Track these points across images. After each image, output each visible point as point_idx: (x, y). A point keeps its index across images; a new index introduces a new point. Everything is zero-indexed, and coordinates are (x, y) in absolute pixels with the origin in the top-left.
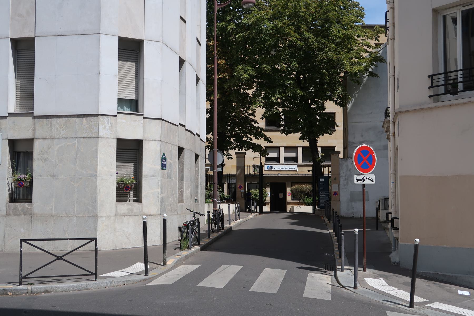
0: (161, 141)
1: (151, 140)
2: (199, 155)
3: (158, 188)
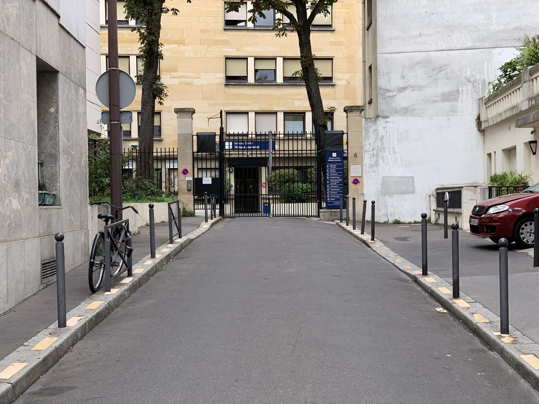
2: (58, 72)
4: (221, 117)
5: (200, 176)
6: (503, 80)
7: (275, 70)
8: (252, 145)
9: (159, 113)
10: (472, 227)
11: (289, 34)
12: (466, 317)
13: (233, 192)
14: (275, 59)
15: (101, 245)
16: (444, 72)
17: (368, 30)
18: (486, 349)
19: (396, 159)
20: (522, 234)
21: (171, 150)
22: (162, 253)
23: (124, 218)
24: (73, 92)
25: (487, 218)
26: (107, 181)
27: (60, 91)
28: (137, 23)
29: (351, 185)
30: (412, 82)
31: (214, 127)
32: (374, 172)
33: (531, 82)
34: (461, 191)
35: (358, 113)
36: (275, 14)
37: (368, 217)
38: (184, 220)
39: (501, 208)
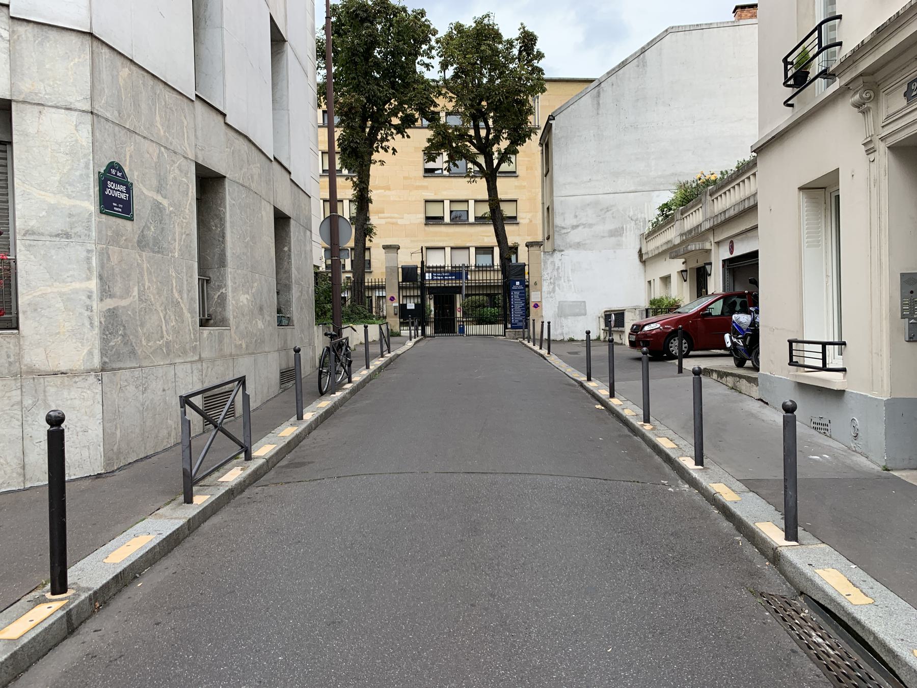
0: (92, 113)
1: (50, 104)
2: (290, 218)
3: (89, 279)
4: (422, 252)
5: (405, 303)
6: (660, 219)
7: (468, 211)
8: (448, 276)
9: (369, 249)
10: (630, 342)
11: (478, 179)
12: (618, 412)
13: (432, 316)
14: (467, 201)
15: (327, 359)
16: (610, 212)
17: (546, 176)
18: (631, 435)
19: (570, 286)
20: (671, 347)
21: (380, 280)
22: (375, 365)
23: (344, 336)
24: (302, 234)
25: (643, 334)
26: (329, 306)
27: (292, 234)
28: (349, 172)
29: (532, 309)
30: (583, 221)
31: (416, 261)
32: (551, 297)
33: (682, 221)
34: (624, 313)
35: (537, 248)
36: (467, 164)
37: (545, 336)
38: (392, 339)
39: (653, 326)
